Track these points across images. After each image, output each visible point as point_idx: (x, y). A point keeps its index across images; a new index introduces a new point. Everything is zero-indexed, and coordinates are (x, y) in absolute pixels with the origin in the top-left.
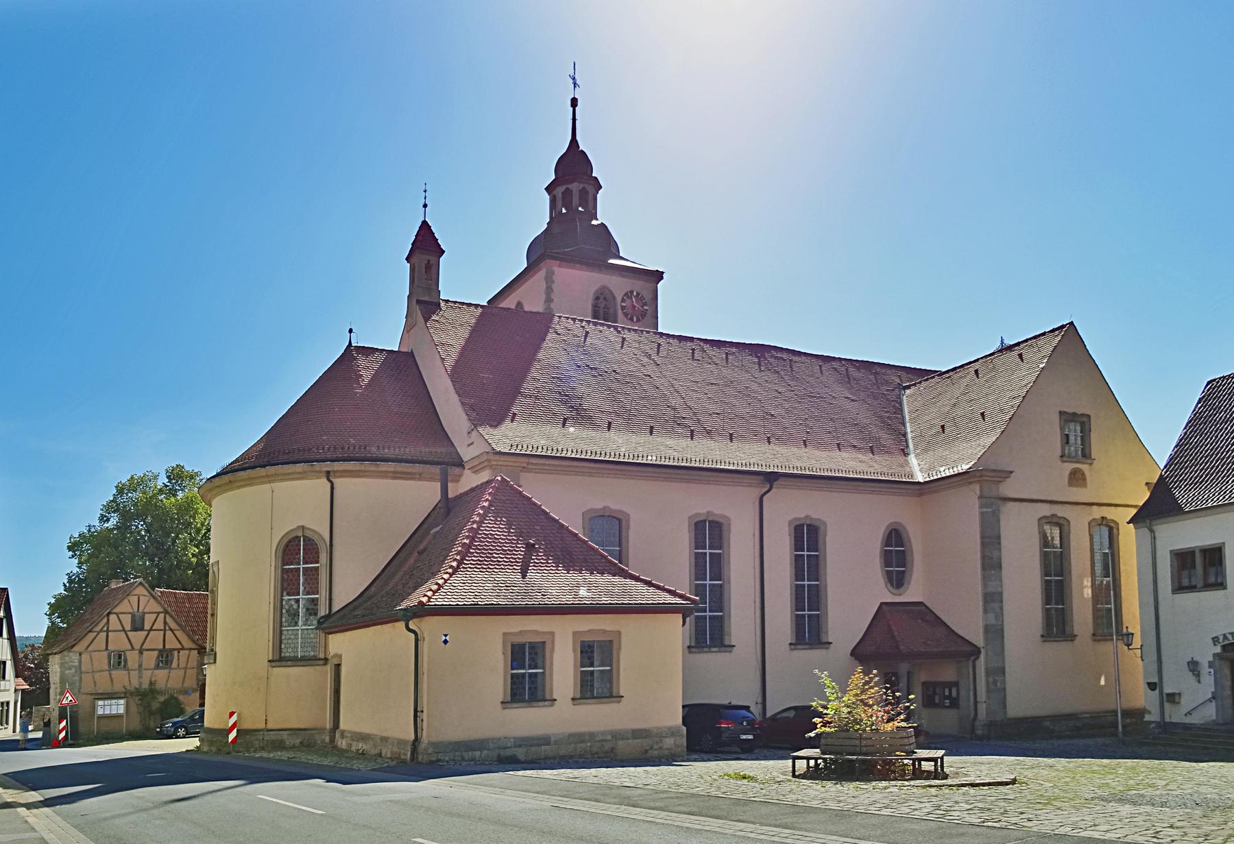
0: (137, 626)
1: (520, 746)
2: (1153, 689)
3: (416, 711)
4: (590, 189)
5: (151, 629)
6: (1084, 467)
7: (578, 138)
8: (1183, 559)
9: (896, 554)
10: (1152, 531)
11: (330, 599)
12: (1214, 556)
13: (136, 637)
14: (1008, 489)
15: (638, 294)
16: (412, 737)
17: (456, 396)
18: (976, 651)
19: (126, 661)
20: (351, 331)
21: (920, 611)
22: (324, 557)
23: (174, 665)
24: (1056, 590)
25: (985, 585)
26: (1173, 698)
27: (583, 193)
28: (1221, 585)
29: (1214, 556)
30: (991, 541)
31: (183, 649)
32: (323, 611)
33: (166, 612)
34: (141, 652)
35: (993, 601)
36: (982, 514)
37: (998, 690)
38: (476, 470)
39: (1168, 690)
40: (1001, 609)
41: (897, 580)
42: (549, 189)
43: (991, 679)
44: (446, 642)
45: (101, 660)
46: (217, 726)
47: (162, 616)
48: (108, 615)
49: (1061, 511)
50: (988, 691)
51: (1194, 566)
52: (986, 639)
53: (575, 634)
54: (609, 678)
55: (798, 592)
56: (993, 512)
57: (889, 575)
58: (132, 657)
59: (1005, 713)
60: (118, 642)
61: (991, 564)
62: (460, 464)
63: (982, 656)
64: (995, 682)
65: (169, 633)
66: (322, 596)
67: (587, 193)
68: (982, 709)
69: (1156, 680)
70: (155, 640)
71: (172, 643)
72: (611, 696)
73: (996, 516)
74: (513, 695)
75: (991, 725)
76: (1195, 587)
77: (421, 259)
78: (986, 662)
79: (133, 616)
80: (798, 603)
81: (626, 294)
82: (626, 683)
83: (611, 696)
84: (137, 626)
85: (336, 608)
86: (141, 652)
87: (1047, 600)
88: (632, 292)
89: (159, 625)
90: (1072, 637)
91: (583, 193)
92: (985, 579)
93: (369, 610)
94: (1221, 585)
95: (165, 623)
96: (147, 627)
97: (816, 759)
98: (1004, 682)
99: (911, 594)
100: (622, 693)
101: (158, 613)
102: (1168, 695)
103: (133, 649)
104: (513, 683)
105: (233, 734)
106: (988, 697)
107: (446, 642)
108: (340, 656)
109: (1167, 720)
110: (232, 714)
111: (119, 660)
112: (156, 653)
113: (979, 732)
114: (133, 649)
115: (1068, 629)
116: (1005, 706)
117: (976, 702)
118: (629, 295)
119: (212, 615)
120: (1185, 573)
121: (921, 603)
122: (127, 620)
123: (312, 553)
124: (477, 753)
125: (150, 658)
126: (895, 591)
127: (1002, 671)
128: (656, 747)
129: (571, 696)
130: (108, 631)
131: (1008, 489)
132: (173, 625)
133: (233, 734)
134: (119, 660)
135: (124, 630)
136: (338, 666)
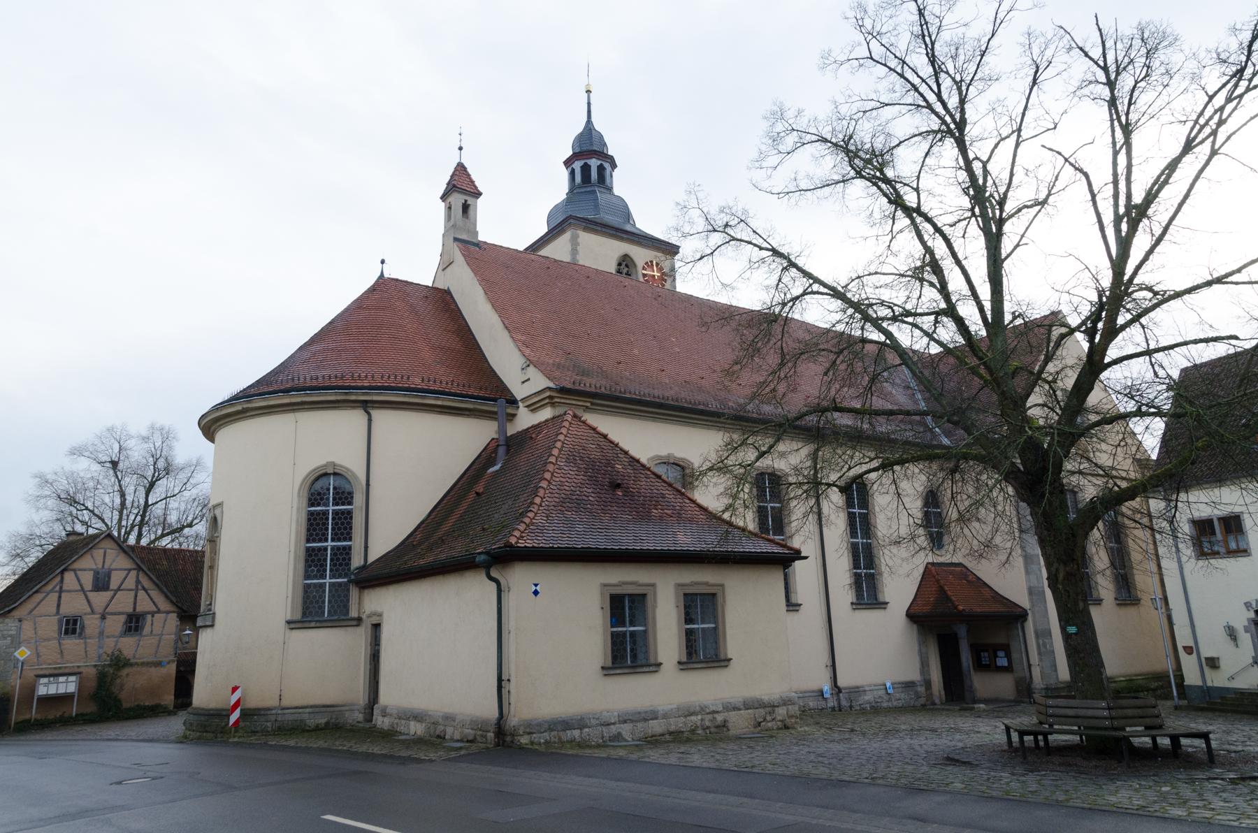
0: (101, 583)
1: (625, 722)
3: (500, 680)
4: (607, 165)
5: (119, 589)
7: (593, 119)
8: (1203, 527)
11: (366, 547)
12: (1233, 524)
13: (100, 599)
16: (497, 715)
17: (506, 333)
18: (1021, 616)
19: (83, 628)
20: (383, 262)
22: (359, 499)
23: (147, 629)
26: (1213, 663)
27: (601, 169)
28: (1244, 552)
29: (1233, 524)
31: (159, 611)
32: (357, 561)
33: (139, 568)
34: (103, 617)
38: (533, 408)
41: (936, 541)
42: (568, 163)
44: (536, 593)
45: (49, 626)
46: (213, 704)
47: (133, 573)
48: (62, 572)
50: (1040, 654)
51: (1213, 533)
52: (1031, 600)
53: (679, 585)
54: (716, 636)
55: (854, 549)
58: (92, 623)
60: (73, 605)
62: (513, 402)
63: (1030, 618)
65: (141, 594)
66: (357, 543)
67: (604, 169)
68: (1036, 672)
69: (1191, 644)
70: (124, 603)
71: (144, 605)
72: (717, 660)
74: (689, 654)
76: (1218, 553)
77: (457, 200)
78: (1035, 625)
79: (96, 573)
82: (733, 645)
83: (717, 660)
84: (101, 583)
85: (371, 559)
86: (103, 617)
89: (130, 582)
90: (882, 605)
91: (601, 169)
93: (416, 562)
94: (1244, 552)
95: (138, 582)
96: (113, 585)
97: (1035, 734)
100: (660, 660)
101: (130, 570)
102: (1207, 659)
103: (93, 612)
104: (614, 643)
105: (234, 717)
106: (1041, 660)
107: (536, 593)
108: (380, 615)
109: (1209, 684)
110: (234, 689)
111: (71, 626)
112: (123, 618)
114: (93, 612)
116: (1056, 670)
117: (1030, 666)
118: (649, 265)
119: (211, 567)
121: (960, 565)
122: (88, 579)
123: (344, 497)
124: (576, 733)
125: (116, 624)
128: (769, 718)
129: (601, 664)
130: (61, 591)
132: (145, 582)
133: (234, 717)
134: (71, 626)
135: (82, 589)
136: (377, 627)
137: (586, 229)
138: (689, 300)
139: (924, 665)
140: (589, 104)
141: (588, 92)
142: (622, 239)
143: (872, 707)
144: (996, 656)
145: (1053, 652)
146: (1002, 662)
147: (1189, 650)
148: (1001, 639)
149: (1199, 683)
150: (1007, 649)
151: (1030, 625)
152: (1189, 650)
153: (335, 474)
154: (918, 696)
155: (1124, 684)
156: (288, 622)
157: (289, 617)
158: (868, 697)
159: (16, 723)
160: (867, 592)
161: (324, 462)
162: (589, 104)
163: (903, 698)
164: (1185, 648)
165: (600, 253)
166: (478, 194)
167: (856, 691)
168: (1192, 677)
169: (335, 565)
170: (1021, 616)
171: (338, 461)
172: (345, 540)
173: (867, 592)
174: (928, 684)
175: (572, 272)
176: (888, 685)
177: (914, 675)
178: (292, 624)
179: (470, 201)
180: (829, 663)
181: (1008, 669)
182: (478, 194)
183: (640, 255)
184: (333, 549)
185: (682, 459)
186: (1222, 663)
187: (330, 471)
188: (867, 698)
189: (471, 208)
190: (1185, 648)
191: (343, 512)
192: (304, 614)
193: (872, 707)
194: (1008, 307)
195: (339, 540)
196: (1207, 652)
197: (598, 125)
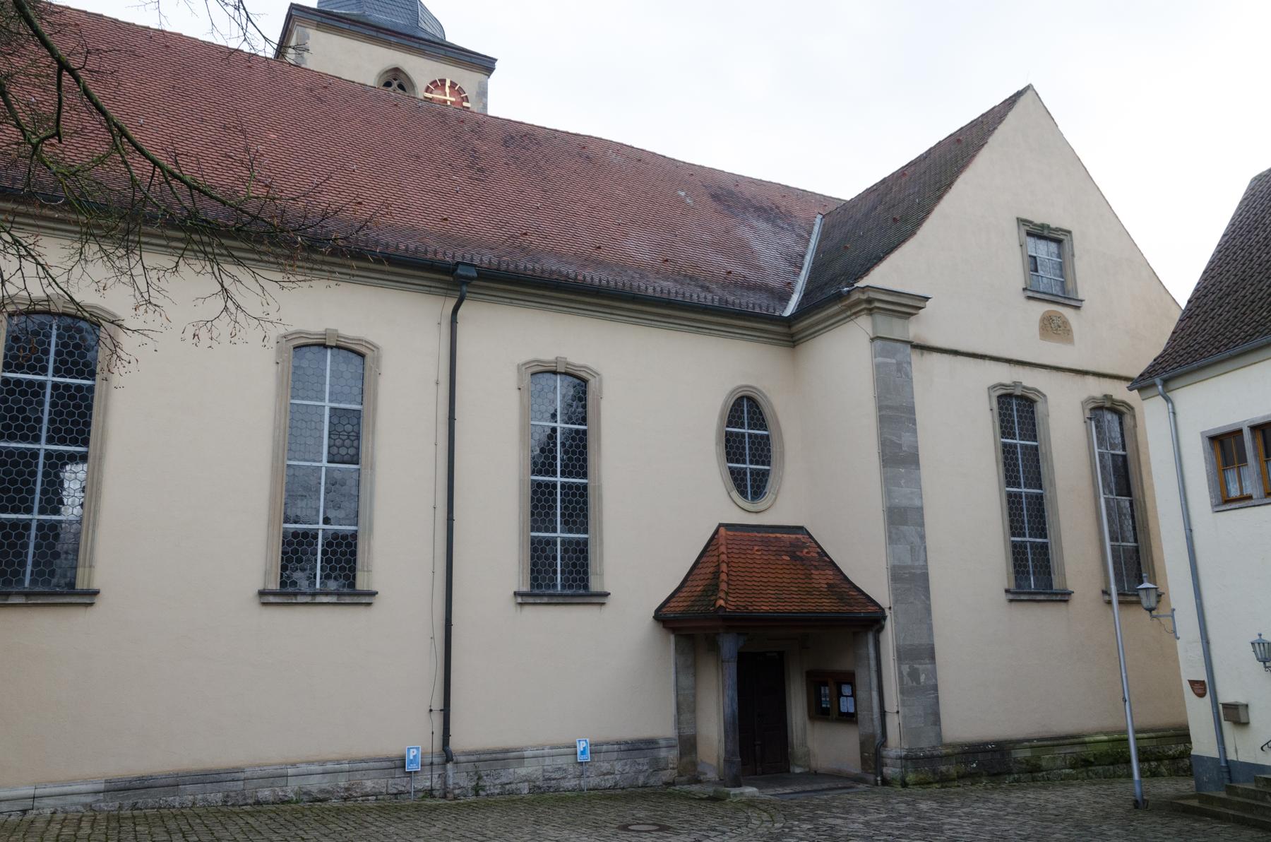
2: (1201, 695)
6: (1068, 313)
9: (748, 441)
10: (1168, 400)
14: (916, 329)
15: (453, 85)
21: (797, 550)
24: (1028, 515)
25: (888, 494)
26: (1235, 715)
30: (896, 415)
35: (905, 523)
36: (878, 367)
37: (924, 691)
39: (1226, 696)
40: (923, 537)
43: (906, 669)
49: (1029, 379)
50: (903, 691)
56: (899, 364)
57: (738, 479)
59: (939, 735)
61: (899, 456)
63: (889, 625)
64: (914, 675)
68: (893, 723)
69: (1202, 676)
73: (903, 370)
75: (911, 759)
76: (1250, 497)
80: (540, 502)
81: (434, 83)
87: (1015, 528)
88: (443, 81)
90: (1063, 597)
92: (888, 483)
98: (933, 674)
99: (781, 508)
102: (1226, 706)
109: (1231, 756)
113: (889, 771)
115: (1056, 585)
116: (937, 720)
117: (883, 713)
120: (1231, 475)
126: (747, 505)
127: (930, 653)
131: (916, 329)
137: (320, 26)
138: (521, 138)
139: (686, 707)
142: (388, 44)
143: (535, 789)
144: (840, 694)
145: (935, 688)
146: (847, 705)
147: (1199, 688)
148: (844, 665)
149: (1214, 753)
150: (850, 679)
151: (889, 637)
152: (1199, 688)
154: (657, 766)
155: (1104, 747)
156: (516, 594)
157: (516, 589)
158: (527, 770)
159: (917, 669)
160: (561, 570)
163: (620, 770)
164: (1192, 683)
165: (359, 62)
167: (501, 758)
168: (1203, 744)
170: (873, 621)
173: (561, 570)
174: (688, 744)
175: (325, 89)
176: (581, 746)
177: (659, 723)
178: (524, 599)
180: (438, 704)
181: (850, 718)
183: (421, 70)
185: (359, 341)
186: (1254, 716)
188: (522, 771)
190: (1192, 683)
193: (535, 789)
196: (1227, 695)
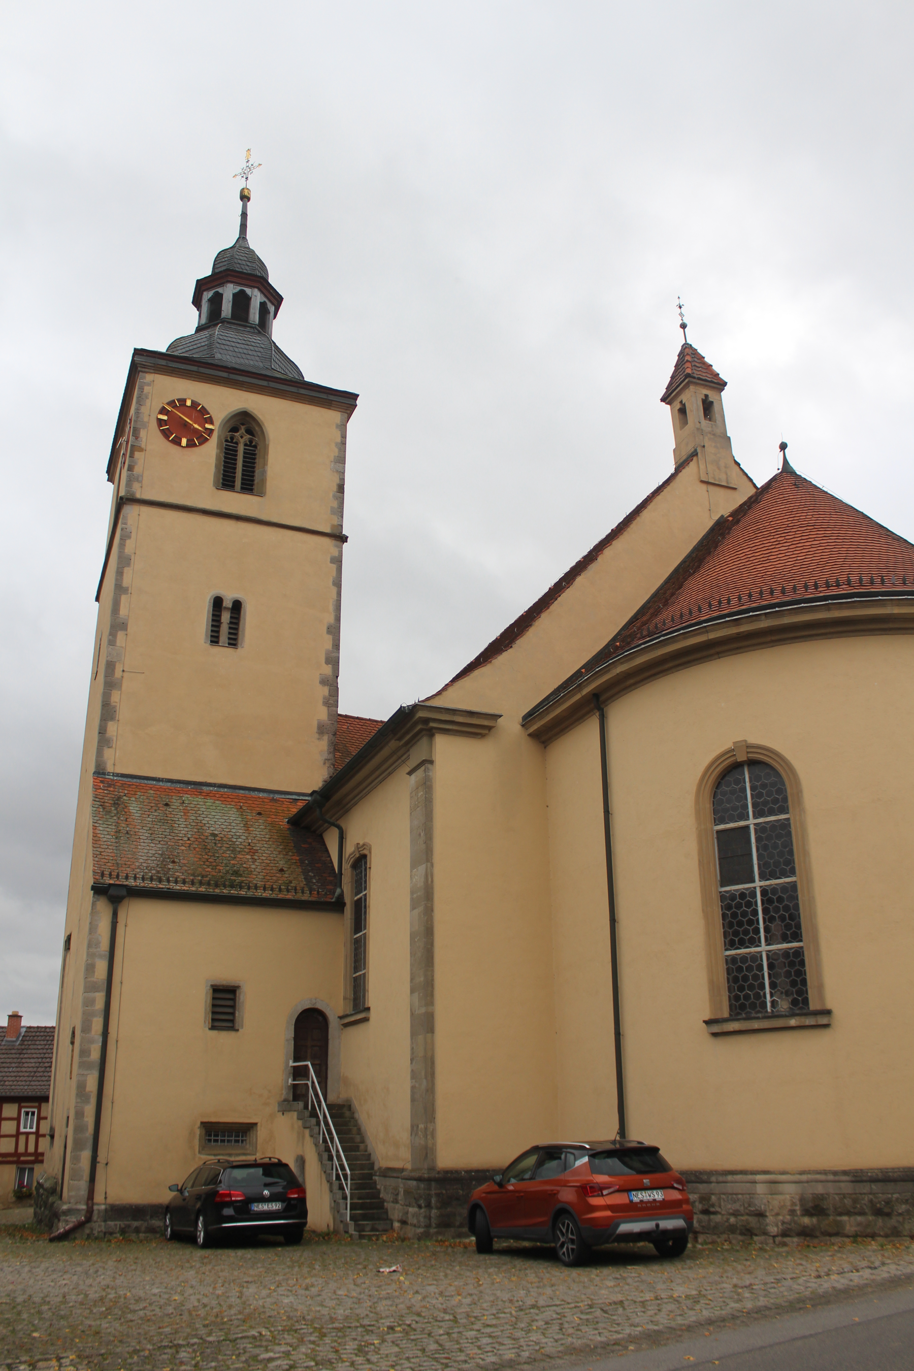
77: (692, 397)
140: (244, 215)
141: (245, 197)
153: (752, 763)
156: (706, 1022)
161: (729, 745)
162: (244, 215)
166: (721, 385)
169: (750, 922)
171: (753, 740)
172: (784, 874)
179: (712, 396)
182: (721, 385)
184: (764, 892)
187: (741, 758)
189: (716, 406)
191: (773, 826)
192: (730, 1015)
194: (99, 1198)
195: (773, 876)
197: (254, 242)
